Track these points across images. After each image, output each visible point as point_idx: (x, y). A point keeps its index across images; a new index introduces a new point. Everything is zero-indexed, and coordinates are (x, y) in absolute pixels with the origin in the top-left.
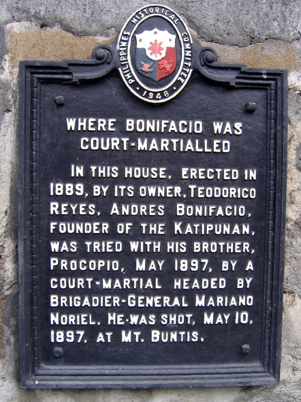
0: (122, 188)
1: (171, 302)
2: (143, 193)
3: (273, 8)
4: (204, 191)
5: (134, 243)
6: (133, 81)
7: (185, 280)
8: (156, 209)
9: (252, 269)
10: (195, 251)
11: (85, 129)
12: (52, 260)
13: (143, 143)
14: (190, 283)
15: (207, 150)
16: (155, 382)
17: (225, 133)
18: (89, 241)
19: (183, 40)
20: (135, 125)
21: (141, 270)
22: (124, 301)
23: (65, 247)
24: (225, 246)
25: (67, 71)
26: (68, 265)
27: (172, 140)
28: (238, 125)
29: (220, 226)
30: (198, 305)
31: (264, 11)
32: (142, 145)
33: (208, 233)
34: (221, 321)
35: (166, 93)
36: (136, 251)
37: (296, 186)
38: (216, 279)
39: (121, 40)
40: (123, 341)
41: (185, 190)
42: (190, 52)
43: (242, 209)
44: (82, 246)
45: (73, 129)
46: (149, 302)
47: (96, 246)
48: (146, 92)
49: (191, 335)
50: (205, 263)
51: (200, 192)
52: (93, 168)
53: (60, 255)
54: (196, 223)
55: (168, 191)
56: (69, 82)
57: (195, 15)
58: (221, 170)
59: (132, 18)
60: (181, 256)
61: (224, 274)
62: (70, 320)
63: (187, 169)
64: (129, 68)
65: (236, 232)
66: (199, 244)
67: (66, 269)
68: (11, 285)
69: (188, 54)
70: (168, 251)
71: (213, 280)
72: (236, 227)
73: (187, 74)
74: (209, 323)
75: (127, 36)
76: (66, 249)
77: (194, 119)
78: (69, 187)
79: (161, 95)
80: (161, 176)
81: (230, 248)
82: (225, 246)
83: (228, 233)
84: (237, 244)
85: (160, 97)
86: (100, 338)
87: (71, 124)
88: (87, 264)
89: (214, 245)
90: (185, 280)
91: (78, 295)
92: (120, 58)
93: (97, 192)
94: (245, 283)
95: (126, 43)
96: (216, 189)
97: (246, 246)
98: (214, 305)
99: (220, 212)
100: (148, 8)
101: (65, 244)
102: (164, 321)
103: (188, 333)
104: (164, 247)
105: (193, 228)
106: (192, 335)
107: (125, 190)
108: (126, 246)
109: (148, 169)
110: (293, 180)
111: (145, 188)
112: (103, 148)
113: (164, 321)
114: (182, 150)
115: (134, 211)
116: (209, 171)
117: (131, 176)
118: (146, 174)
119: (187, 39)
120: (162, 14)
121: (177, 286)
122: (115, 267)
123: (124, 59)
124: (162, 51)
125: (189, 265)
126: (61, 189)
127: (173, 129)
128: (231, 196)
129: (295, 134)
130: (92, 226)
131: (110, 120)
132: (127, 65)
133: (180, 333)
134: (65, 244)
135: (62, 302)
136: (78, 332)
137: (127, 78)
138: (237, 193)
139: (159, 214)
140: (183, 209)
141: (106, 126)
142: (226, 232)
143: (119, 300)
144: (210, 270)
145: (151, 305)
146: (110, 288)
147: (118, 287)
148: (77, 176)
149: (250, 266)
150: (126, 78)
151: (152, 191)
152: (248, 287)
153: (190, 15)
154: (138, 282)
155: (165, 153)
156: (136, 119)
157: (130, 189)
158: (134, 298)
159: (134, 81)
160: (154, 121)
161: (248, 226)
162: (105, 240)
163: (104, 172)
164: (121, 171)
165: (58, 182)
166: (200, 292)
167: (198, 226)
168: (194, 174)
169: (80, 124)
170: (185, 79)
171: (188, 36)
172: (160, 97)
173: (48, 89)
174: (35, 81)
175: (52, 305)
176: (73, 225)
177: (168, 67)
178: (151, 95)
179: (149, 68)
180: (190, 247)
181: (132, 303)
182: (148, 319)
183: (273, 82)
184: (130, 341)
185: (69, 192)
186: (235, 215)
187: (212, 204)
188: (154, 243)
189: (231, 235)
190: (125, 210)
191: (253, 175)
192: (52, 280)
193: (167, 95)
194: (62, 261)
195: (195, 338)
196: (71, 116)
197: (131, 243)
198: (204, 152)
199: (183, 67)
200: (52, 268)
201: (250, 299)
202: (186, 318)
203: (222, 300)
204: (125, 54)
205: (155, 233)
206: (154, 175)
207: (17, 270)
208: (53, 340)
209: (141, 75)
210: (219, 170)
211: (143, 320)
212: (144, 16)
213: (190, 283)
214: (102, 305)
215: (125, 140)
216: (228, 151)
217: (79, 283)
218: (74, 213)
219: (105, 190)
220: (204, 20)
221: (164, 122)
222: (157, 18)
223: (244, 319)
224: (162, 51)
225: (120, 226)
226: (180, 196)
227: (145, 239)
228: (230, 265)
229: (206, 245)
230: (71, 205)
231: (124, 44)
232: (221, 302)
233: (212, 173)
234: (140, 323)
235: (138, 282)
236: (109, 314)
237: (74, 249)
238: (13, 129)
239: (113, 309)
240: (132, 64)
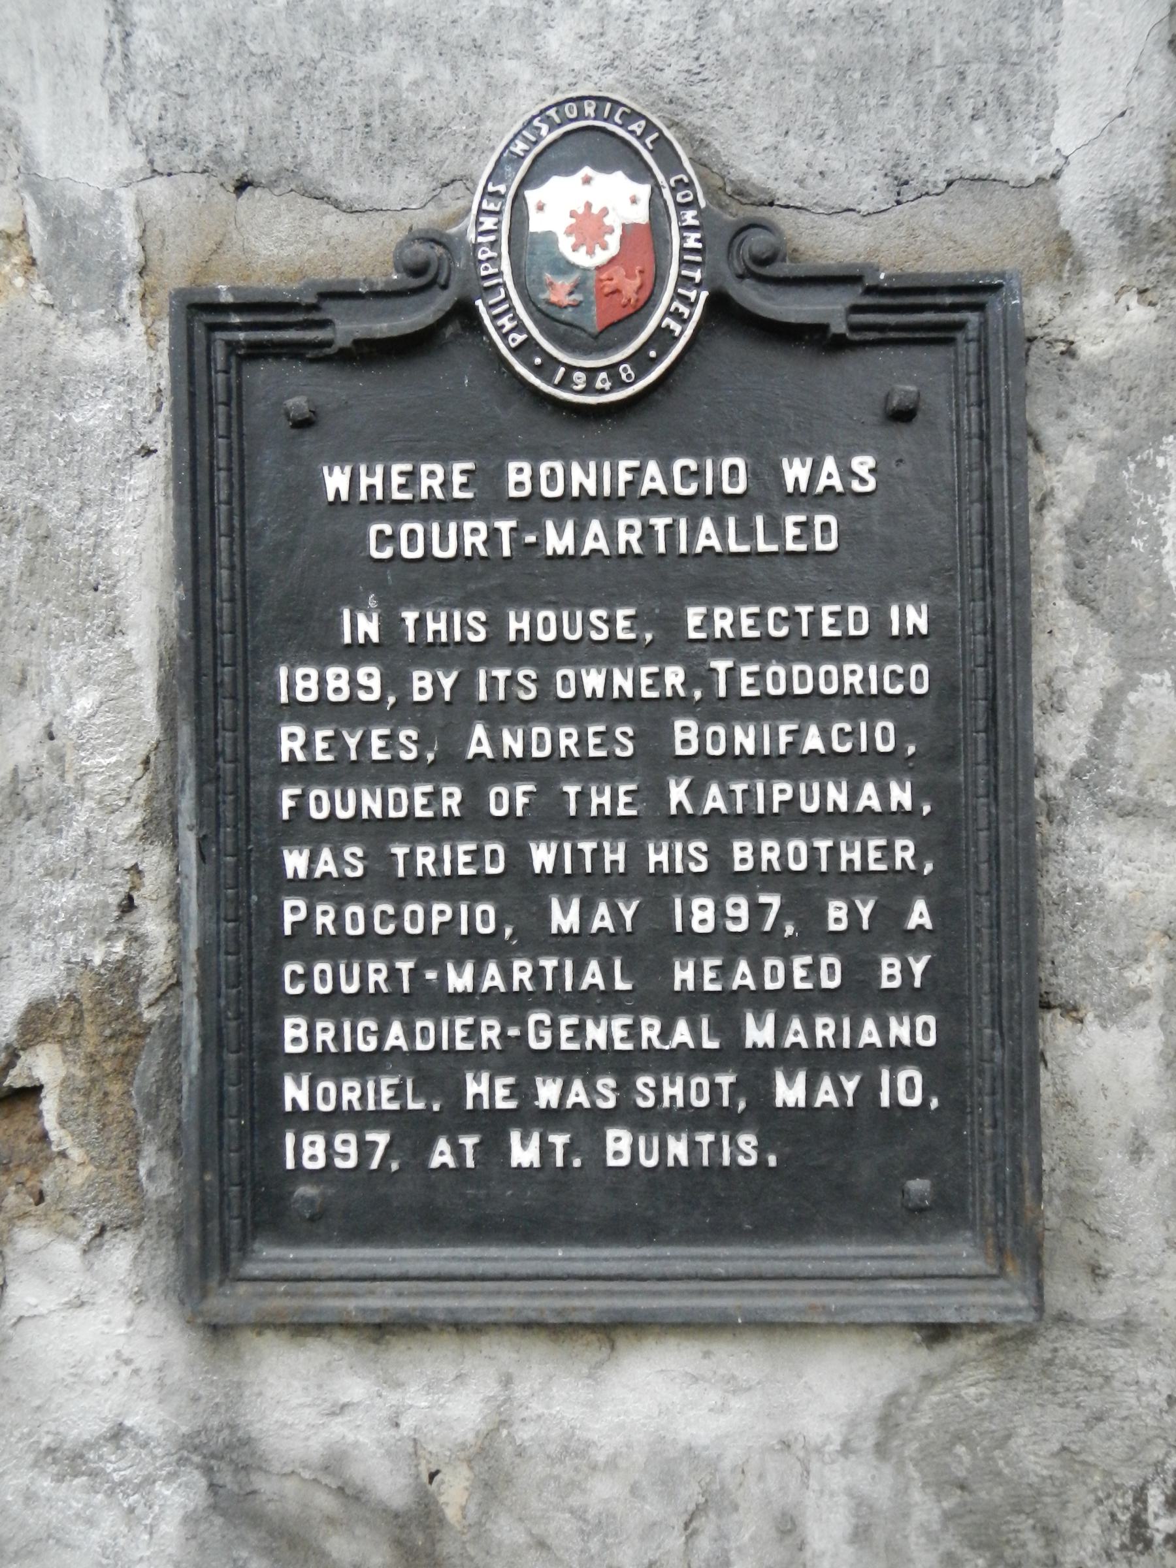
0: (502, 674)
1: (665, 1035)
2: (566, 688)
3: (969, 79)
4: (759, 676)
5: (543, 846)
6: (521, 338)
7: (708, 963)
8: (607, 738)
9: (929, 926)
10: (738, 867)
11: (379, 495)
12: (288, 904)
13: (560, 532)
14: (725, 972)
15: (762, 547)
16: (619, 1303)
17: (820, 489)
18: (403, 841)
19: (674, 198)
20: (535, 478)
21: (566, 930)
22: (513, 1032)
23: (326, 864)
24: (834, 851)
25: (316, 316)
26: (339, 920)
27: (653, 521)
28: (862, 464)
29: (816, 787)
30: (755, 1045)
31: (938, 89)
32: (559, 541)
33: (776, 809)
34: (832, 1098)
35: (627, 371)
36: (549, 870)
37: (1067, 654)
38: (808, 960)
39: (480, 211)
40: (514, 1164)
41: (699, 676)
42: (698, 235)
43: (885, 729)
44: (379, 859)
45: (344, 496)
46: (596, 1034)
47: (425, 858)
48: (562, 370)
49: (733, 1142)
50: (770, 905)
51: (746, 681)
52: (410, 617)
53: (311, 887)
54: (739, 778)
55: (645, 682)
56: (328, 351)
57: (714, 124)
58: (810, 608)
59: (512, 140)
60: (691, 884)
61: (834, 942)
62: (346, 1096)
63: (703, 610)
64: (507, 298)
65: (868, 803)
66: (749, 845)
67: (332, 931)
68: (163, 989)
69: (691, 243)
70: (652, 870)
71: (800, 962)
72: (869, 789)
73: (692, 305)
74: (791, 1104)
75: (496, 195)
76: (331, 868)
77: (718, 453)
78: (337, 678)
79: (609, 376)
80: (621, 635)
81: (850, 855)
82: (834, 851)
83: (844, 807)
84: (872, 843)
85: (608, 385)
86: (442, 1155)
87: (336, 481)
88: (398, 915)
89: (797, 849)
90: (708, 963)
91: (368, 1014)
92: (477, 268)
93: (422, 690)
94: (907, 971)
95: (494, 220)
96: (796, 668)
97: (905, 851)
98: (805, 1045)
99: (813, 741)
100: (559, 104)
101: (326, 854)
102: (645, 1098)
103: (726, 1140)
104: (636, 855)
105: (729, 795)
106: (737, 1147)
107: (511, 680)
108: (519, 857)
109: (579, 614)
110: (1059, 636)
111: (571, 674)
112: (437, 552)
113: (645, 1098)
114: (683, 549)
115: (541, 746)
116: (771, 612)
117: (527, 638)
118: (572, 630)
119: (686, 196)
120: (606, 120)
121: (684, 982)
122: (485, 923)
123: (491, 271)
124: (607, 238)
125: (720, 913)
126: (313, 684)
127: (653, 486)
128: (847, 691)
129: (1059, 485)
130: (411, 797)
131: (458, 467)
132: (502, 290)
133: (698, 1138)
134: (326, 854)
135: (320, 1037)
136: (370, 1137)
137: (505, 330)
138: (865, 681)
139: (619, 752)
140: (692, 736)
141: (446, 485)
142: (835, 805)
143: (497, 1030)
144: (789, 930)
145: (603, 1045)
146: (470, 990)
147: (496, 988)
148: (361, 640)
149: (919, 915)
150: (499, 329)
151: (594, 681)
152: (917, 983)
153: (699, 123)
154: (558, 971)
155: (631, 563)
156: (536, 458)
157: (527, 677)
158: (548, 1022)
159: (525, 336)
160: (592, 466)
161: (908, 785)
162: (449, 839)
163: (442, 626)
164: (496, 624)
165: (303, 663)
166: (760, 1000)
167: (745, 786)
168: (726, 624)
169: (365, 481)
170: (684, 322)
171: (690, 185)
172: (608, 385)
173: (261, 374)
174: (220, 354)
175: (289, 1048)
176: (351, 794)
177: (630, 287)
178: (580, 378)
179: (571, 293)
180: (720, 856)
181: (540, 1039)
182: (591, 1090)
183: (973, 318)
184: (537, 1165)
185: (338, 690)
186: (864, 748)
187: (789, 718)
188: (607, 845)
189: (850, 814)
190: (513, 743)
191: (918, 619)
192: (288, 970)
193: (629, 376)
194: (320, 909)
195: (747, 1156)
196: (338, 458)
197: (533, 846)
198: (754, 554)
199: (677, 286)
200: (288, 931)
201: (926, 1027)
202: (715, 1088)
203: (832, 1028)
204: (495, 254)
205: (608, 812)
206: (599, 631)
207: (177, 943)
208: (290, 1164)
209: (547, 316)
210: (804, 610)
211: (578, 1094)
212: (550, 131)
213: (725, 972)
214: (445, 1047)
215: (505, 526)
216: (832, 546)
217: (372, 978)
218: (353, 757)
219: (447, 683)
220: (743, 135)
221: (624, 464)
222: (590, 134)
223: (910, 1093)
224: (607, 238)
225: (498, 795)
226: (682, 693)
227: (577, 831)
228: (853, 913)
229: (771, 849)
230: (345, 734)
231: (489, 223)
232: (829, 1033)
233: (785, 619)
234: (569, 1105)
235: (558, 971)
236: (469, 1077)
237: (354, 868)
238: (162, 507)
239: (479, 1059)
240: (516, 284)
